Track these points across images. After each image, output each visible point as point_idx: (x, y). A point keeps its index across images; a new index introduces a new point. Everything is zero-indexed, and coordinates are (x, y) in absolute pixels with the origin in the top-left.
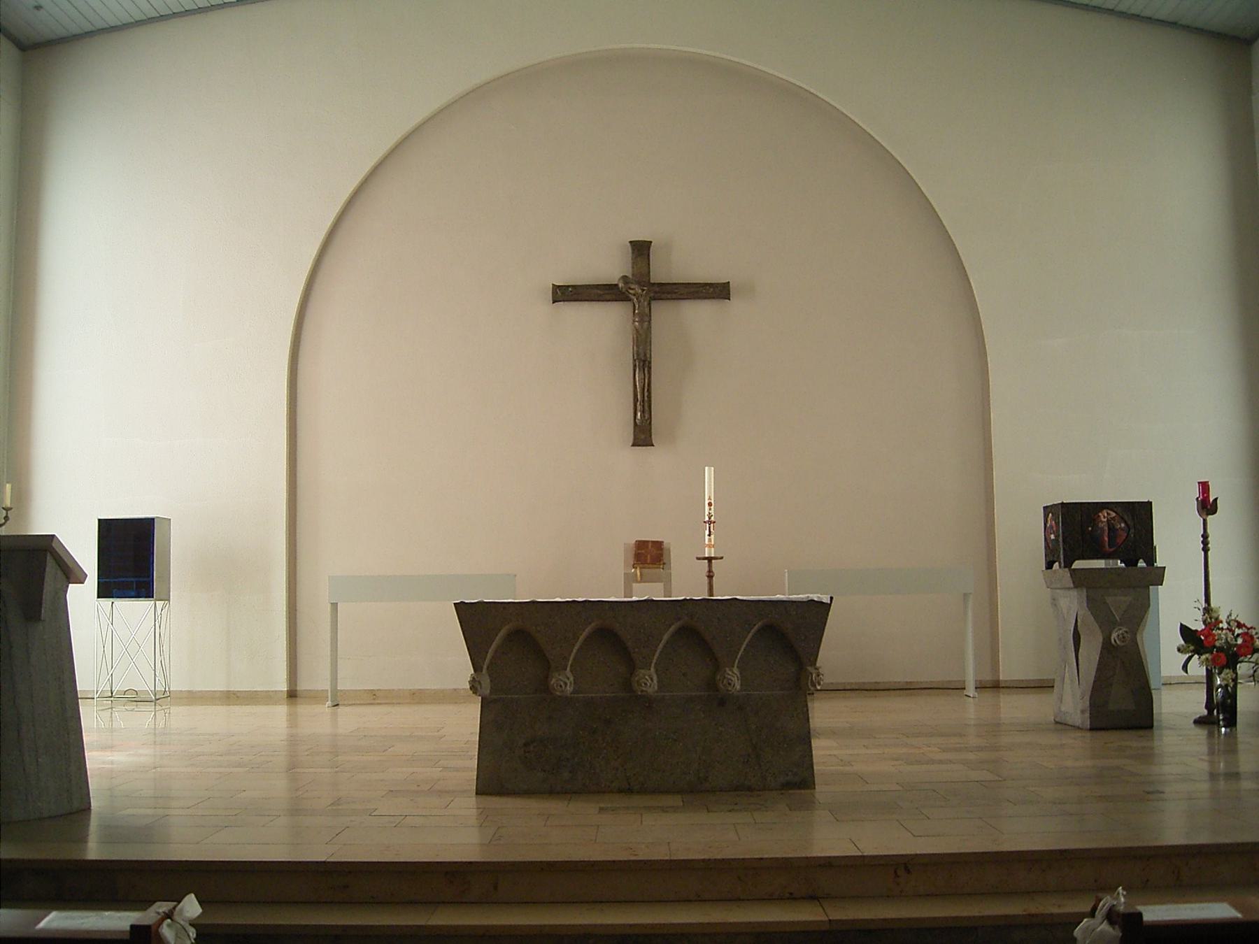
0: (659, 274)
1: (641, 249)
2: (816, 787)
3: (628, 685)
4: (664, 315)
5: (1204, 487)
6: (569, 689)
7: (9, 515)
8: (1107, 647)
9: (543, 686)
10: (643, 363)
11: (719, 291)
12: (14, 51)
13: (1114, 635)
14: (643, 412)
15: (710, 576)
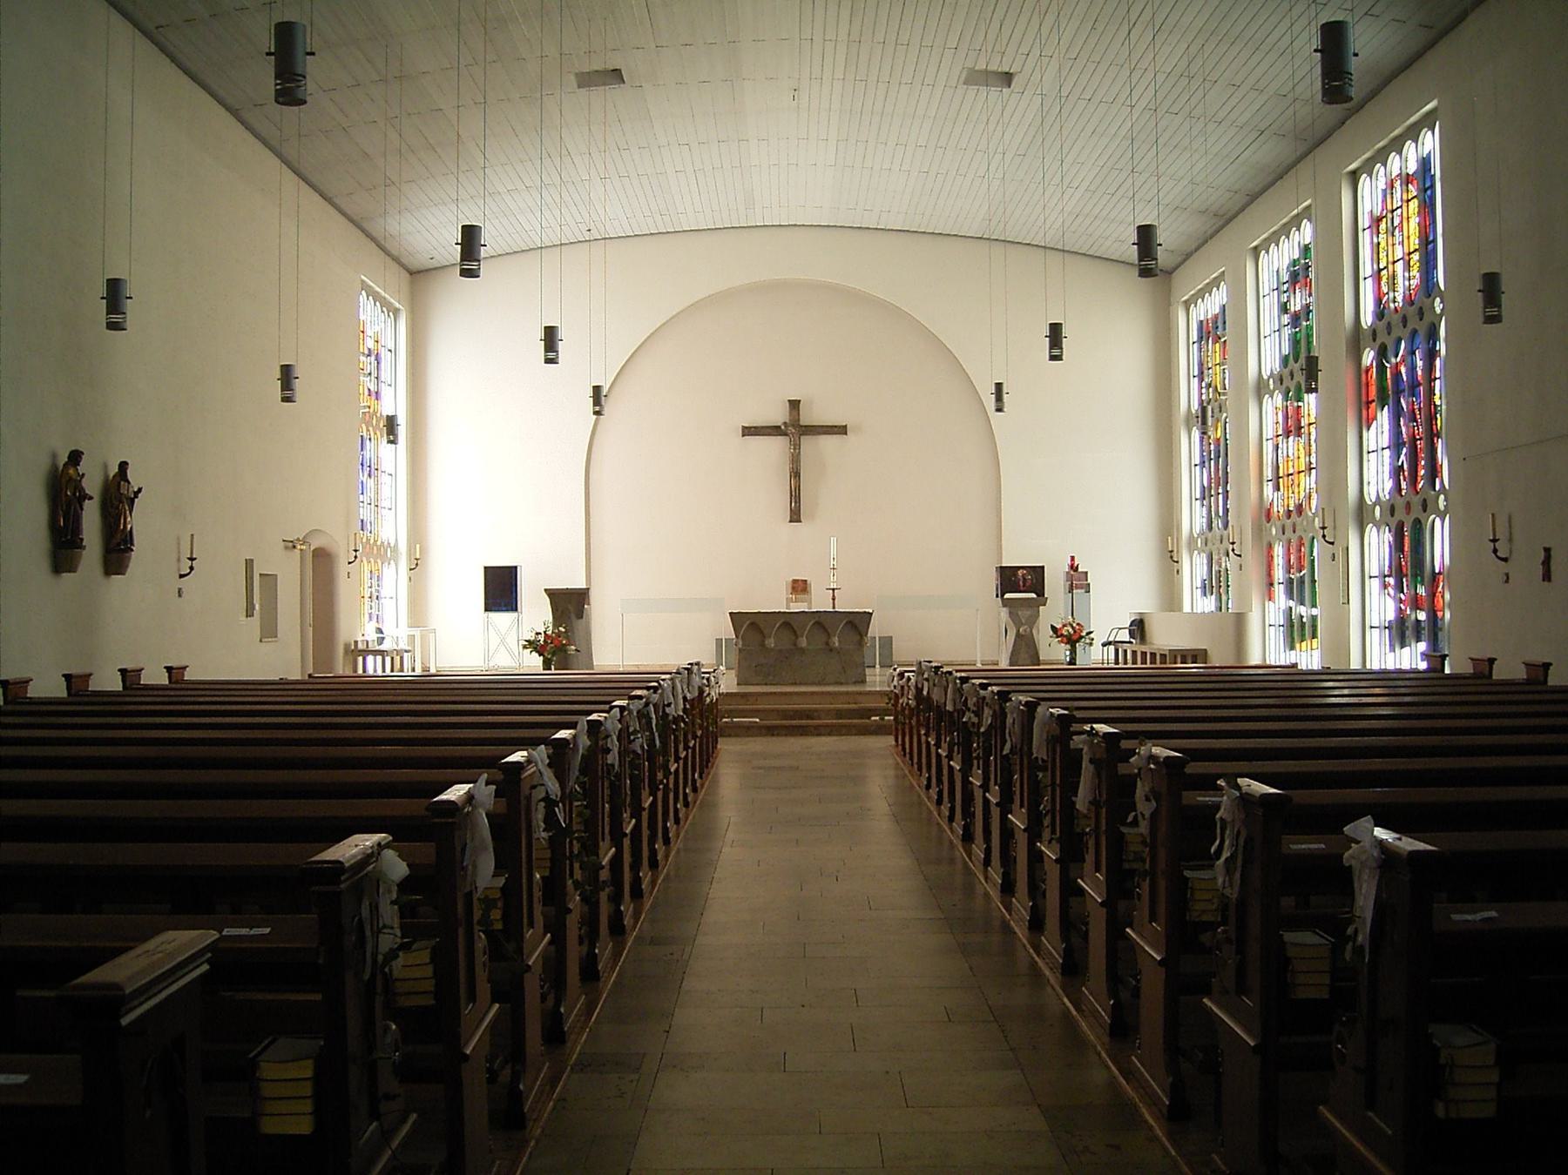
0: (805, 420)
1: (794, 405)
2: (293, 20)
3: (795, 645)
4: (807, 443)
5: (1073, 558)
6: (773, 645)
8: (1018, 635)
9: (763, 645)
10: (796, 474)
11: (842, 430)
12: (408, 275)
13: (1021, 630)
14: (796, 502)
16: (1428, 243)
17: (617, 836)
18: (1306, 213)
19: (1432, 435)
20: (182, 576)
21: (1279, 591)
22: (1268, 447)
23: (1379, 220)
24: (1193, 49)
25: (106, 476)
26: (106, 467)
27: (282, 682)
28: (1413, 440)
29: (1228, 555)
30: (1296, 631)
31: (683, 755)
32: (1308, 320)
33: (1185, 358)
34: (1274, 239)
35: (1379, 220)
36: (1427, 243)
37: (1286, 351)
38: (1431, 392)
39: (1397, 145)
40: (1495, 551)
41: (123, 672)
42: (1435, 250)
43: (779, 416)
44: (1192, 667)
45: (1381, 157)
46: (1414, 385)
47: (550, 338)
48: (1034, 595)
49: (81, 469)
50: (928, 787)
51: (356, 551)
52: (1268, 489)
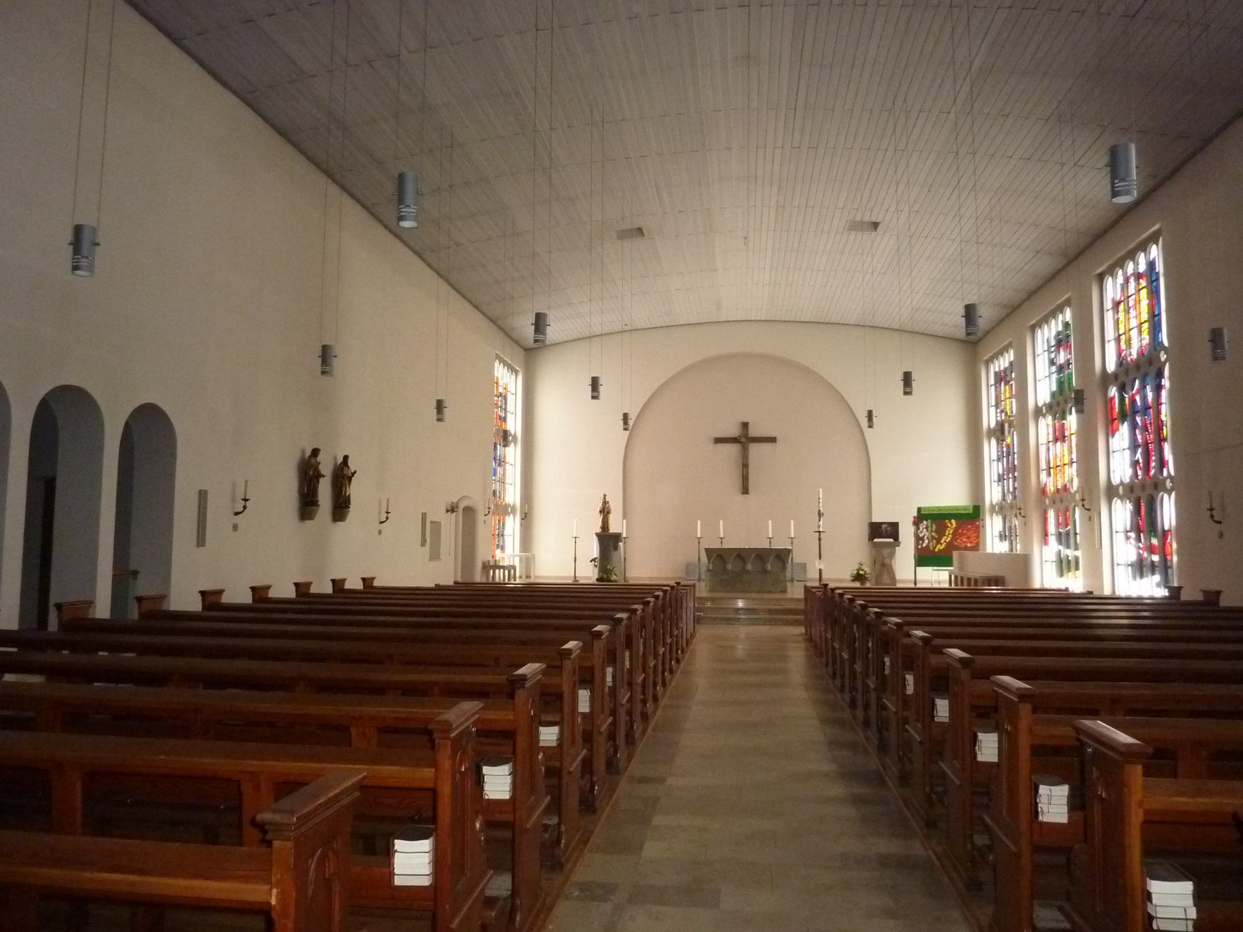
0: (753, 432)
1: (745, 425)
3: (744, 568)
4: (754, 448)
7: (247, 505)
11: (772, 440)
12: (523, 352)
15: (820, 539)
16: (1155, 316)
17: (656, 655)
18: (1068, 303)
19: (1161, 440)
20: (381, 523)
21: (1052, 539)
22: (1043, 450)
23: (1118, 303)
24: (994, 201)
25: (336, 463)
26: (335, 458)
27: (438, 587)
28: (1146, 444)
29: (1016, 517)
30: (1064, 565)
31: (669, 641)
32: (1069, 369)
33: (987, 396)
34: (1045, 320)
35: (1118, 303)
36: (1154, 317)
37: (1054, 388)
38: (1159, 412)
39: (1132, 255)
40: (1212, 516)
41: (333, 581)
42: (1160, 320)
43: (734, 431)
44: (994, 590)
45: (1120, 263)
46: (1146, 408)
47: (595, 384)
48: (892, 540)
49: (319, 459)
50: (827, 665)
51: (489, 508)
52: (1043, 476)
